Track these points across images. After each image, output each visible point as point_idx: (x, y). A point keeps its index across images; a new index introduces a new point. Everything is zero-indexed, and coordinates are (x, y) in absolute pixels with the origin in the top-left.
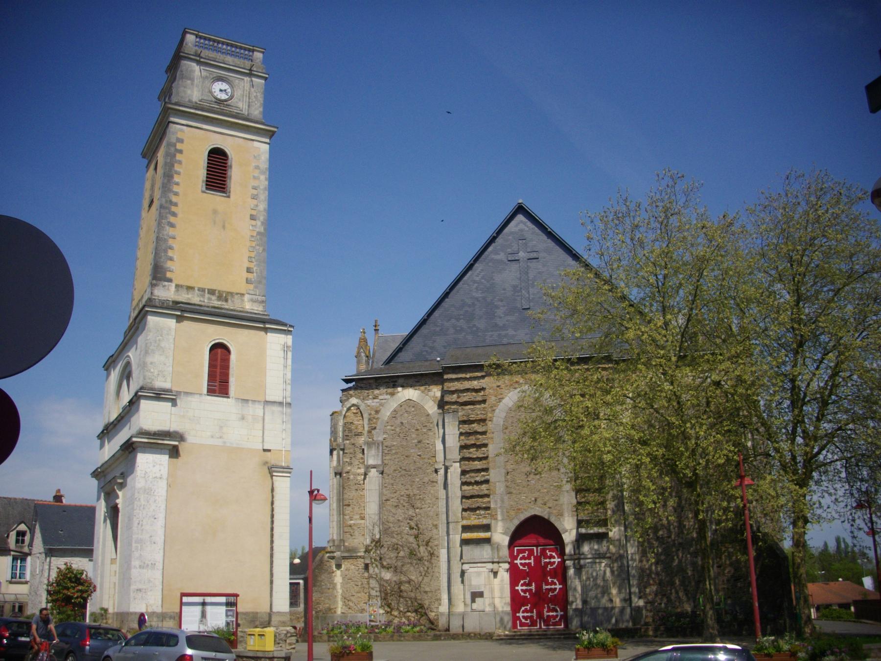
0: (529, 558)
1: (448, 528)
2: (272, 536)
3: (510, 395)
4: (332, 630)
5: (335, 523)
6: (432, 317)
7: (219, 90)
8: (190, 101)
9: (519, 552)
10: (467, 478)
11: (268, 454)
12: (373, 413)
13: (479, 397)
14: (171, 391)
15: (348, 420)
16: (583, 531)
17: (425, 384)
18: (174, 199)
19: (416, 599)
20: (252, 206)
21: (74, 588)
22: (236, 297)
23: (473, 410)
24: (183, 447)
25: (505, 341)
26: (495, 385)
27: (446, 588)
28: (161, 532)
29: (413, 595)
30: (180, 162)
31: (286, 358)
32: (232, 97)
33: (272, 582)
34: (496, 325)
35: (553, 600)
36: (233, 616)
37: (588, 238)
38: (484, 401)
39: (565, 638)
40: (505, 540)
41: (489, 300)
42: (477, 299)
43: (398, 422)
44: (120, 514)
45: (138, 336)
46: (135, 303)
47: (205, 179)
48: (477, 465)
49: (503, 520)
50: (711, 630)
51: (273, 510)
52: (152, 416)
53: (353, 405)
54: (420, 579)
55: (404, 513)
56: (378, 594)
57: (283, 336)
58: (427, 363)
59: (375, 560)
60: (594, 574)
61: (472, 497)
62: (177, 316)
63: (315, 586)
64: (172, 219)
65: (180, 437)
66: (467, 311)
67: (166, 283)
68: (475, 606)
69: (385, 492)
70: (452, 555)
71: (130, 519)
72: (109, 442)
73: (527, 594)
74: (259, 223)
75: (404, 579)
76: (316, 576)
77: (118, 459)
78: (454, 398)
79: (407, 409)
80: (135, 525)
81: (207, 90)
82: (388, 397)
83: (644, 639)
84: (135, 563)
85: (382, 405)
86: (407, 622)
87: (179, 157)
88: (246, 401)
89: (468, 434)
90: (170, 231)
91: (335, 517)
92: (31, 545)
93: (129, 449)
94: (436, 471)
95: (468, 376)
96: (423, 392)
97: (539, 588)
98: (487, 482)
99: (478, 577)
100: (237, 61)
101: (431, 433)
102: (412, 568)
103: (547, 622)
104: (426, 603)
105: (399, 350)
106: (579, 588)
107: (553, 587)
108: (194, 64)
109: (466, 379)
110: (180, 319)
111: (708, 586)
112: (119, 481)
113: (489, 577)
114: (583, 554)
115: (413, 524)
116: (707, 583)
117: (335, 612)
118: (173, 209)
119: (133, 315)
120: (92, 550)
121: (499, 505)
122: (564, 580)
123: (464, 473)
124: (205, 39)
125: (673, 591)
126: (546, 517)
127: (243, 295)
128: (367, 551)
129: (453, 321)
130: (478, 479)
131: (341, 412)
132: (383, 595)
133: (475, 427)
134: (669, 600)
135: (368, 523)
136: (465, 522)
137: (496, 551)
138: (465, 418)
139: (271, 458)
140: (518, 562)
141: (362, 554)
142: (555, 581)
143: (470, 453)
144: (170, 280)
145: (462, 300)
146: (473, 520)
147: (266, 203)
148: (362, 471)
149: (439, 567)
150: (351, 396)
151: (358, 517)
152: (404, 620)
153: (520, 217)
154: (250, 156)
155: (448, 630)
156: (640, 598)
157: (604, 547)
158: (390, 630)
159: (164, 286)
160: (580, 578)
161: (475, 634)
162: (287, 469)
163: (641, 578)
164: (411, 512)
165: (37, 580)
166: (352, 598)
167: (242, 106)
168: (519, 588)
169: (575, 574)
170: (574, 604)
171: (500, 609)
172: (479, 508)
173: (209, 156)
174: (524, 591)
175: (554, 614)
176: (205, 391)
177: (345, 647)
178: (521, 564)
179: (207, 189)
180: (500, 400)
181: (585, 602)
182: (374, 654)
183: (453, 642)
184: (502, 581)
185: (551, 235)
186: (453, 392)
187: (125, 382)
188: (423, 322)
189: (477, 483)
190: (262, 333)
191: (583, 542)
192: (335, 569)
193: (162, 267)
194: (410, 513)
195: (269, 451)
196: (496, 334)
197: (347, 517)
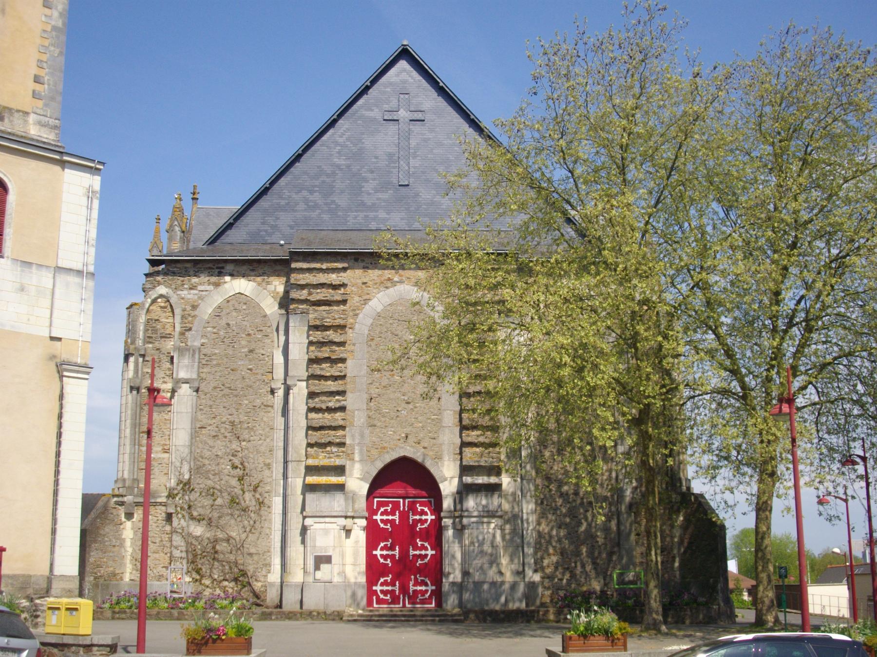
0: (393, 513)
1: (285, 468)
2: (58, 464)
3: (379, 296)
4: (118, 603)
5: (127, 457)
6: (276, 186)
9: (380, 504)
10: (316, 402)
11: (58, 343)
12: (189, 308)
13: (337, 295)
15: (153, 316)
16: (468, 480)
17: (263, 274)
19: (236, 563)
22: (16, 115)
23: (328, 312)
25: (373, 225)
26: (360, 281)
27: (279, 550)
29: (232, 558)
31: (90, 208)
33: (54, 532)
34: (363, 204)
35: (423, 570)
37: (535, 78)
38: (344, 302)
39: (440, 621)
40: (364, 488)
41: (355, 169)
42: (338, 167)
43: (223, 322)
48: (331, 386)
49: (361, 461)
50: (654, 616)
51: (60, 426)
53: (161, 296)
54: (244, 536)
55: (226, 447)
56: (184, 555)
57: (88, 175)
58: (268, 247)
59: (182, 508)
60: (481, 538)
61: (321, 428)
63: (95, 541)
66: (324, 182)
68: (319, 575)
69: (200, 417)
70: (290, 505)
73: (389, 561)
74: (56, 14)
75: (220, 535)
76: (98, 528)
78: (304, 294)
79: (237, 306)
82: (211, 287)
83: (544, 624)
86: (222, 595)
88: (29, 264)
89: (321, 344)
91: (128, 448)
94: (272, 392)
95: (324, 266)
96: (259, 284)
97: (404, 553)
98: (343, 409)
99: (326, 535)
101: (267, 341)
102: (233, 522)
103: (413, 599)
104: (250, 569)
105: (229, 226)
106: (458, 556)
107: (423, 552)
109: (321, 270)
111: (654, 557)
113: (340, 537)
114: (467, 511)
115: (237, 462)
116: (653, 553)
117: (121, 579)
121: (357, 441)
122: (438, 544)
123: (312, 395)
125: (579, 564)
126: (420, 460)
128: (171, 495)
129: (305, 193)
130: (331, 404)
131: (143, 304)
133: (331, 335)
134: (573, 576)
135: (175, 458)
136: (310, 462)
137: (350, 502)
138: (318, 323)
139: (62, 351)
140: (378, 517)
141: (164, 500)
142: (426, 544)
143: (321, 369)
145: (319, 167)
146: (322, 459)
148: (169, 386)
149: (270, 521)
150: (159, 283)
151: (160, 449)
152: (218, 591)
153: (403, 64)
155: (280, 606)
156: (536, 571)
157: (495, 501)
158: (200, 604)
160: (461, 542)
161: (319, 613)
162: (86, 368)
163: (538, 546)
164: (235, 445)
168: (378, 552)
169: (454, 536)
170: (452, 576)
171: (352, 580)
172: (330, 444)
174: (385, 557)
175: (424, 588)
177: (209, 630)
178: (382, 521)
180: (366, 301)
181: (466, 574)
182: (254, 641)
183: (287, 622)
184: (357, 542)
185: (443, 92)
186: (302, 287)
188: (264, 191)
189: (329, 410)
190: (57, 168)
191: (467, 495)
192: (123, 519)
195: (60, 339)
196: (362, 215)
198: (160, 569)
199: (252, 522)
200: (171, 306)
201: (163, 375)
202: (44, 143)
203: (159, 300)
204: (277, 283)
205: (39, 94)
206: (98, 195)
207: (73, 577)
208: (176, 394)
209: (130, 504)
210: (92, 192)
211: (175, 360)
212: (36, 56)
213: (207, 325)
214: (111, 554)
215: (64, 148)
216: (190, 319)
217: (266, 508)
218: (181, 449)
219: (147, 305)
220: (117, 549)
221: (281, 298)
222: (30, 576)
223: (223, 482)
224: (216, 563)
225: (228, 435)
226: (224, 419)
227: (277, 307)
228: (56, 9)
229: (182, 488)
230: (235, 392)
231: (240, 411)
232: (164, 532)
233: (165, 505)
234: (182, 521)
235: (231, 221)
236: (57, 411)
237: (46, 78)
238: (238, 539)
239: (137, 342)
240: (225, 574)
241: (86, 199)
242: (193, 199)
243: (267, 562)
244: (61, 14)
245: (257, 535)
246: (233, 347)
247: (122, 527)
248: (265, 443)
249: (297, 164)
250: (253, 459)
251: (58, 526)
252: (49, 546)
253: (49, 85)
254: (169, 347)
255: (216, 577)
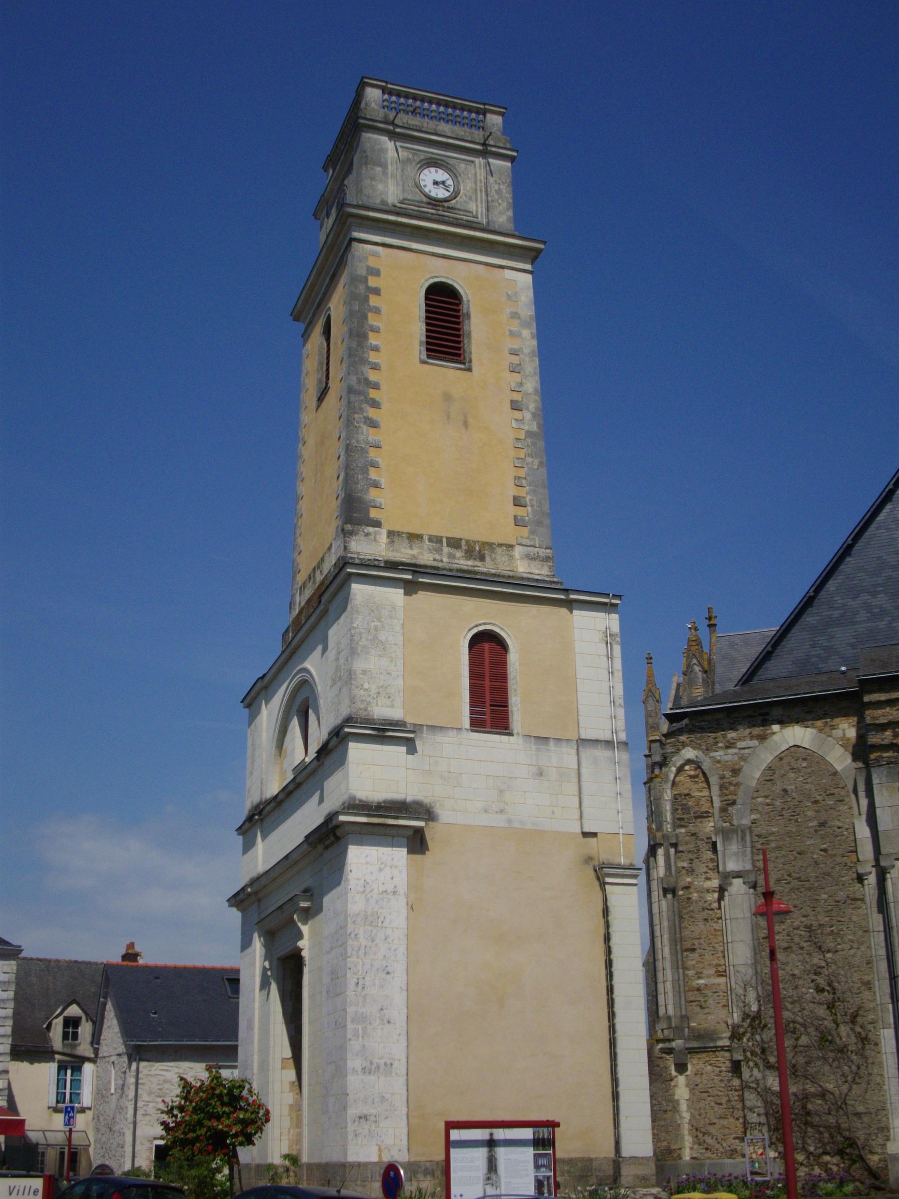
2: (611, 1003)
7: (433, 182)
8: (384, 202)
11: (593, 841)
12: (728, 774)
14: (404, 724)
17: (824, 716)
18: (373, 376)
19: (838, 1128)
20: (513, 385)
21: (228, 1116)
22: (499, 550)
24: (433, 834)
28: (400, 1000)
29: (832, 1120)
30: (377, 311)
31: (610, 657)
32: (456, 194)
33: (615, 1097)
36: (547, 1167)
43: (778, 788)
44: (306, 970)
45: (329, 627)
46: (301, 578)
47: (424, 339)
52: (371, 773)
53: (689, 762)
55: (804, 962)
56: (763, 1119)
58: (824, 678)
59: (753, 1053)
62: (406, 582)
64: (372, 413)
65: (426, 812)
67: (371, 529)
71: (337, 976)
72: (264, 838)
74: (528, 416)
75: (811, 1089)
77: (296, 863)
79: (793, 764)
80: (351, 986)
81: (411, 183)
82: (755, 742)
84: (354, 1063)
85: (743, 758)
86: (824, 1175)
87: (373, 301)
90: (372, 435)
92: (96, 1039)
93: (329, 839)
94: (860, 879)
96: (821, 731)
100: (460, 131)
101: (843, 808)
102: (827, 1068)
104: (861, 1136)
105: (766, 656)
108: (384, 139)
110: (410, 588)
112: (303, 904)
115: (822, 982)
117: (680, 1157)
118: (373, 394)
119: (301, 600)
120: (236, 1048)
124: (399, 94)
127: (510, 547)
128: (736, 1035)
129: (865, 597)
132: (773, 1122)
139: (600, 850)
141: (726, 1042)
144: (377, 524)
145: (879, 558)
147: (537, 378)
148: (715, 883)
149: (880, 1064)
150: (684, 745)
152: (817, 1171)
154: (501, 298)
159: (367, 535)
164: (816, 960)
165: (113, 1105)
166: (712, 1129)
167: (476, 208)
173: (427, 299)
176: (467, 723)
179: (429, 357)
186: (883, 727)
187: (295, 723)
190: (564, 611)
192: (674, 1073)
193: (360, 500)
194: (815, 961)
195: (594, 835)
197: (691, 973)
198: (731, 1140)
199: (854, 1068)
200: (704, 774)
201: (705, 869)
202: (537, 581)
203: (687, 768)
204: (846, 726)
205: (523, 520)
206: (618, 639)
207: (346, 1155)
208: (726, 893)
209: (680, 1052)
210: (611, 635)
211: (719, 847)
212: (513, 472)
213: (755, 794)
214: (662, 1123)
215: (561, 583)
216: (732, 788)
217: (872, 1046)
218: (742, 969)
219: (672, 776)
220: (669, 1115)
221: (854, 747)
222: (590, 1160)
223: (805, 1012)
224: (809, 1129)
225: (805, 945)
226: (797, 923)
227: (849, 759)
228: (528, 409)
229: (750, 1025)
230: (807, 884)
231: (819, 909)
232: (732, 1088)
233: (729, 1049)
234: (756, 1072)
235: (769, 649)
236: (602, 931)
237: (528, 498)
238: (837, 1093)
239: (664, 827)
240: (824, 1145)
241: (604, 646)
242: (709, 626)
243: (883, 1125)
244: (534, 415)
245: (864, 1086)
246: (796, 821)
247: (673, 1084)
248: (859, 953)
249: (848, 559)
250: (845, 976)
251: (621, 1089)
252: (611, 1117)
253: (532, 506)
254: (708, 830)
255: (812, 1149)
